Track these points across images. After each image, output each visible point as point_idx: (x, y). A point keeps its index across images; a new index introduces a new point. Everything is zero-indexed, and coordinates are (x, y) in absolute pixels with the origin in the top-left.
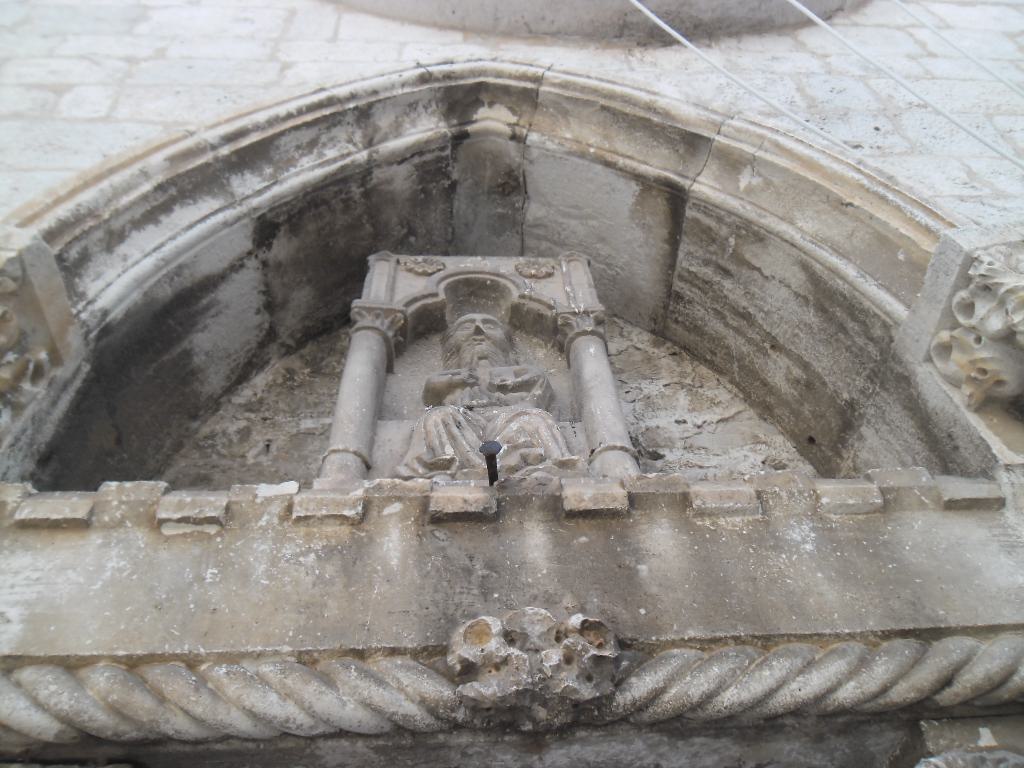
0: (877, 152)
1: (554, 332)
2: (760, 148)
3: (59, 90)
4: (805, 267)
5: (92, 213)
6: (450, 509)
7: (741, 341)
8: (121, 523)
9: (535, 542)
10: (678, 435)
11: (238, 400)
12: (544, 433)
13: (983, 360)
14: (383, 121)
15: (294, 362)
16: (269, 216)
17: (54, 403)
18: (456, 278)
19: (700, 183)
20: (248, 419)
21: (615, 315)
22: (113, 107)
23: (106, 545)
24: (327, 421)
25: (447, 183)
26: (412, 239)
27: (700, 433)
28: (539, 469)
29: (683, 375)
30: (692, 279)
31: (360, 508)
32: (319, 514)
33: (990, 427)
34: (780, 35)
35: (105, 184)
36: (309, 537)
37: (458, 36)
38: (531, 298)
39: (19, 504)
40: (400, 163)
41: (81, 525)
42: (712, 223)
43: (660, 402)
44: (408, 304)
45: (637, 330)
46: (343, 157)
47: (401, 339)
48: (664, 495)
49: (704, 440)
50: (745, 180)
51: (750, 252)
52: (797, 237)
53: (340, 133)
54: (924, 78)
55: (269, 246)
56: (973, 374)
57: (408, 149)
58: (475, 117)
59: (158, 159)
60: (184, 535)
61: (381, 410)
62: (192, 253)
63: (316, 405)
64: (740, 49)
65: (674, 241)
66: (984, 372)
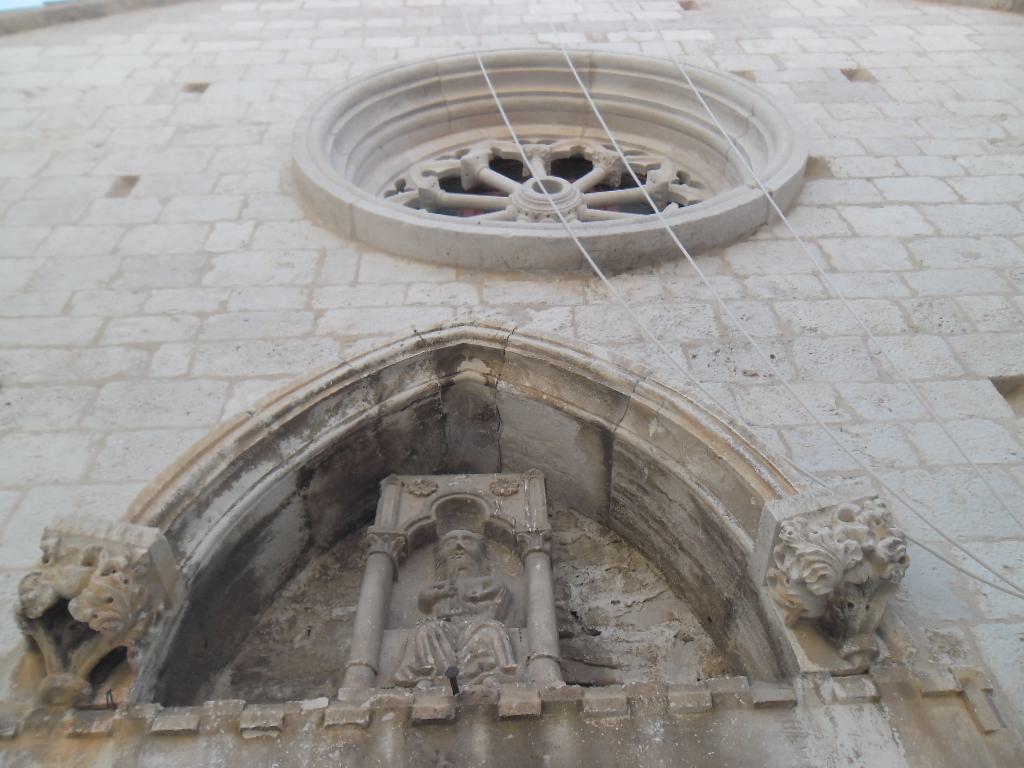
0: (769, 381)
1: (515, 544)
2: (662, 406)
3: (151, 348)
4: (694, 500)
5: (188, 493)
6: (426, 716)
7: (660, 539)
8: (216, 731)
9: (479, 738)
10: (612, 615)
11: (286, 594)
12: (497, 644)
13: (791, 596)
14: (389, 381)
15: (328, 559)
16: (308, 466)
17: (167, 635)
18: (445, 499)
19: (621, 427)
20: (295, 610)
21: (572, 508)
22: (191, 365)
23: (209, 746)
24: (352, 609)
25: (439, 416)
26: (415, 457)
27: (630, 612)
28: (490, 675)
29: (621, 560)
30: (624, 491)
31: (367, 718)
32: (341, 722)
33: (799, 640)
34: (710, 256)
35: (195, 469)
36: (335, 738)
37: (451, 273)
38: (498, 518)
39: (153, 720)
40: (402, 410)
41: (192, 734)
42: (632, 458)
43: (602, 585)
44: (407, 529)
45: (589, 521)
46: (361, 413)
47: (404, 554)
48: (565, 702)
49: (631, 618)
50: (653, 428)
51: (659, 481)
52: (687, 477)
53: (358, 395)
54: (820, 299)
55: (308, 486)
56: (787, 604)
57: (408, 400)
58: (458, 369)
59: (229, 442)
60: (258, 738)
61: (388, 619)
62: (252, 508)
63: (344, 596)
64: (675, 274)
65: (608, 467)
66: (792, 603)
